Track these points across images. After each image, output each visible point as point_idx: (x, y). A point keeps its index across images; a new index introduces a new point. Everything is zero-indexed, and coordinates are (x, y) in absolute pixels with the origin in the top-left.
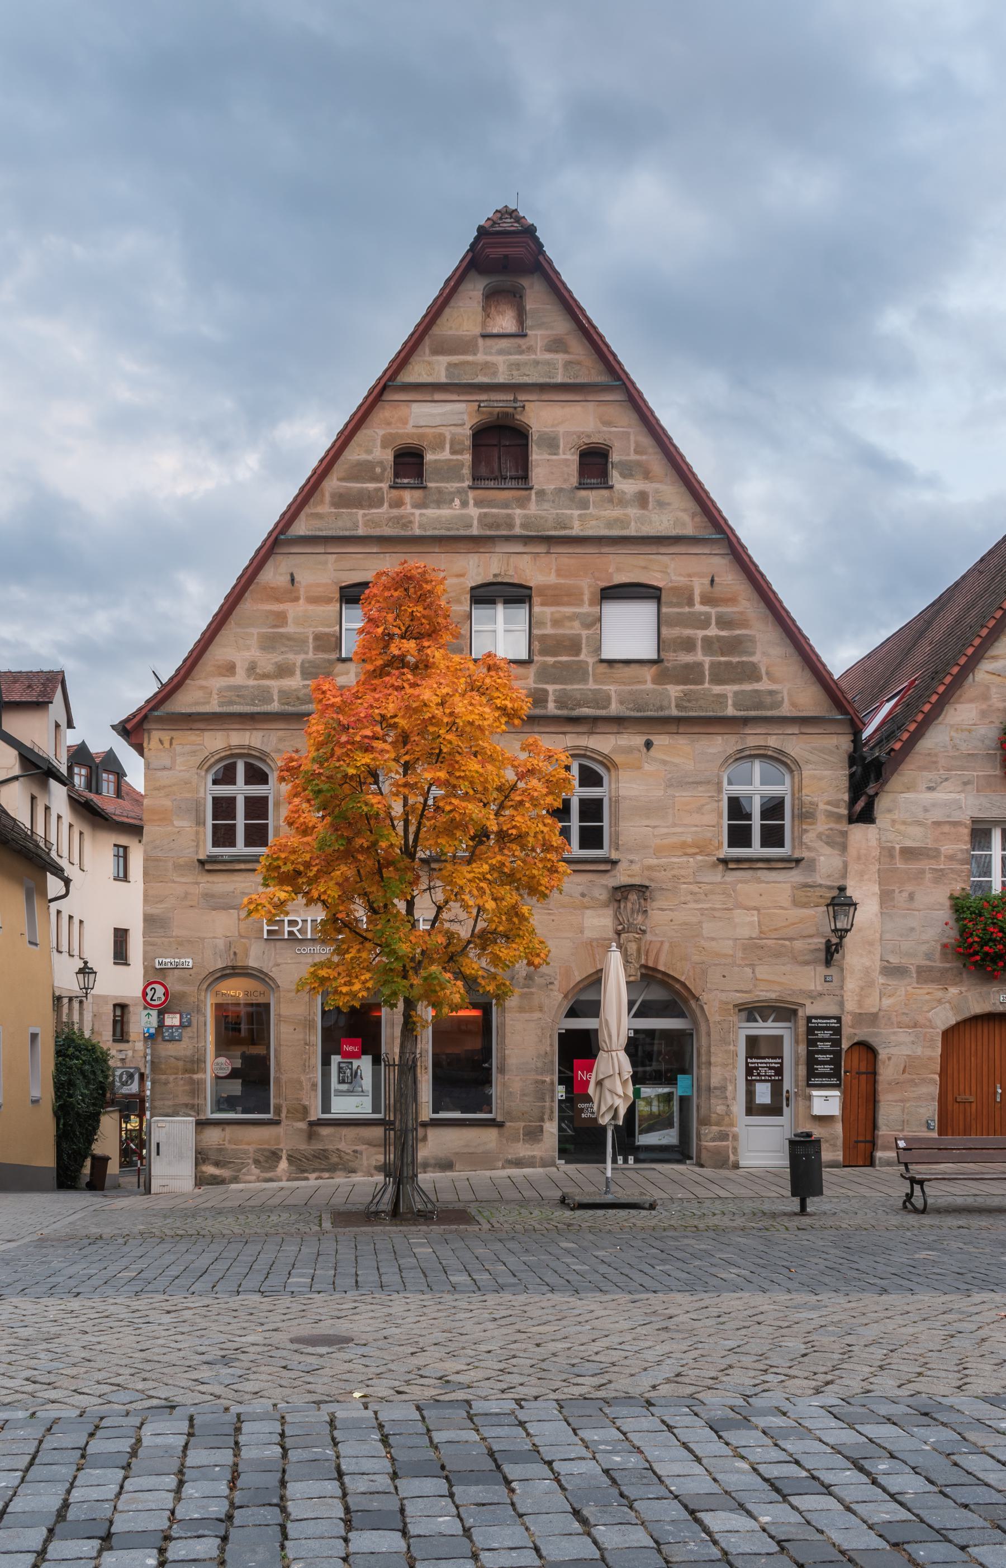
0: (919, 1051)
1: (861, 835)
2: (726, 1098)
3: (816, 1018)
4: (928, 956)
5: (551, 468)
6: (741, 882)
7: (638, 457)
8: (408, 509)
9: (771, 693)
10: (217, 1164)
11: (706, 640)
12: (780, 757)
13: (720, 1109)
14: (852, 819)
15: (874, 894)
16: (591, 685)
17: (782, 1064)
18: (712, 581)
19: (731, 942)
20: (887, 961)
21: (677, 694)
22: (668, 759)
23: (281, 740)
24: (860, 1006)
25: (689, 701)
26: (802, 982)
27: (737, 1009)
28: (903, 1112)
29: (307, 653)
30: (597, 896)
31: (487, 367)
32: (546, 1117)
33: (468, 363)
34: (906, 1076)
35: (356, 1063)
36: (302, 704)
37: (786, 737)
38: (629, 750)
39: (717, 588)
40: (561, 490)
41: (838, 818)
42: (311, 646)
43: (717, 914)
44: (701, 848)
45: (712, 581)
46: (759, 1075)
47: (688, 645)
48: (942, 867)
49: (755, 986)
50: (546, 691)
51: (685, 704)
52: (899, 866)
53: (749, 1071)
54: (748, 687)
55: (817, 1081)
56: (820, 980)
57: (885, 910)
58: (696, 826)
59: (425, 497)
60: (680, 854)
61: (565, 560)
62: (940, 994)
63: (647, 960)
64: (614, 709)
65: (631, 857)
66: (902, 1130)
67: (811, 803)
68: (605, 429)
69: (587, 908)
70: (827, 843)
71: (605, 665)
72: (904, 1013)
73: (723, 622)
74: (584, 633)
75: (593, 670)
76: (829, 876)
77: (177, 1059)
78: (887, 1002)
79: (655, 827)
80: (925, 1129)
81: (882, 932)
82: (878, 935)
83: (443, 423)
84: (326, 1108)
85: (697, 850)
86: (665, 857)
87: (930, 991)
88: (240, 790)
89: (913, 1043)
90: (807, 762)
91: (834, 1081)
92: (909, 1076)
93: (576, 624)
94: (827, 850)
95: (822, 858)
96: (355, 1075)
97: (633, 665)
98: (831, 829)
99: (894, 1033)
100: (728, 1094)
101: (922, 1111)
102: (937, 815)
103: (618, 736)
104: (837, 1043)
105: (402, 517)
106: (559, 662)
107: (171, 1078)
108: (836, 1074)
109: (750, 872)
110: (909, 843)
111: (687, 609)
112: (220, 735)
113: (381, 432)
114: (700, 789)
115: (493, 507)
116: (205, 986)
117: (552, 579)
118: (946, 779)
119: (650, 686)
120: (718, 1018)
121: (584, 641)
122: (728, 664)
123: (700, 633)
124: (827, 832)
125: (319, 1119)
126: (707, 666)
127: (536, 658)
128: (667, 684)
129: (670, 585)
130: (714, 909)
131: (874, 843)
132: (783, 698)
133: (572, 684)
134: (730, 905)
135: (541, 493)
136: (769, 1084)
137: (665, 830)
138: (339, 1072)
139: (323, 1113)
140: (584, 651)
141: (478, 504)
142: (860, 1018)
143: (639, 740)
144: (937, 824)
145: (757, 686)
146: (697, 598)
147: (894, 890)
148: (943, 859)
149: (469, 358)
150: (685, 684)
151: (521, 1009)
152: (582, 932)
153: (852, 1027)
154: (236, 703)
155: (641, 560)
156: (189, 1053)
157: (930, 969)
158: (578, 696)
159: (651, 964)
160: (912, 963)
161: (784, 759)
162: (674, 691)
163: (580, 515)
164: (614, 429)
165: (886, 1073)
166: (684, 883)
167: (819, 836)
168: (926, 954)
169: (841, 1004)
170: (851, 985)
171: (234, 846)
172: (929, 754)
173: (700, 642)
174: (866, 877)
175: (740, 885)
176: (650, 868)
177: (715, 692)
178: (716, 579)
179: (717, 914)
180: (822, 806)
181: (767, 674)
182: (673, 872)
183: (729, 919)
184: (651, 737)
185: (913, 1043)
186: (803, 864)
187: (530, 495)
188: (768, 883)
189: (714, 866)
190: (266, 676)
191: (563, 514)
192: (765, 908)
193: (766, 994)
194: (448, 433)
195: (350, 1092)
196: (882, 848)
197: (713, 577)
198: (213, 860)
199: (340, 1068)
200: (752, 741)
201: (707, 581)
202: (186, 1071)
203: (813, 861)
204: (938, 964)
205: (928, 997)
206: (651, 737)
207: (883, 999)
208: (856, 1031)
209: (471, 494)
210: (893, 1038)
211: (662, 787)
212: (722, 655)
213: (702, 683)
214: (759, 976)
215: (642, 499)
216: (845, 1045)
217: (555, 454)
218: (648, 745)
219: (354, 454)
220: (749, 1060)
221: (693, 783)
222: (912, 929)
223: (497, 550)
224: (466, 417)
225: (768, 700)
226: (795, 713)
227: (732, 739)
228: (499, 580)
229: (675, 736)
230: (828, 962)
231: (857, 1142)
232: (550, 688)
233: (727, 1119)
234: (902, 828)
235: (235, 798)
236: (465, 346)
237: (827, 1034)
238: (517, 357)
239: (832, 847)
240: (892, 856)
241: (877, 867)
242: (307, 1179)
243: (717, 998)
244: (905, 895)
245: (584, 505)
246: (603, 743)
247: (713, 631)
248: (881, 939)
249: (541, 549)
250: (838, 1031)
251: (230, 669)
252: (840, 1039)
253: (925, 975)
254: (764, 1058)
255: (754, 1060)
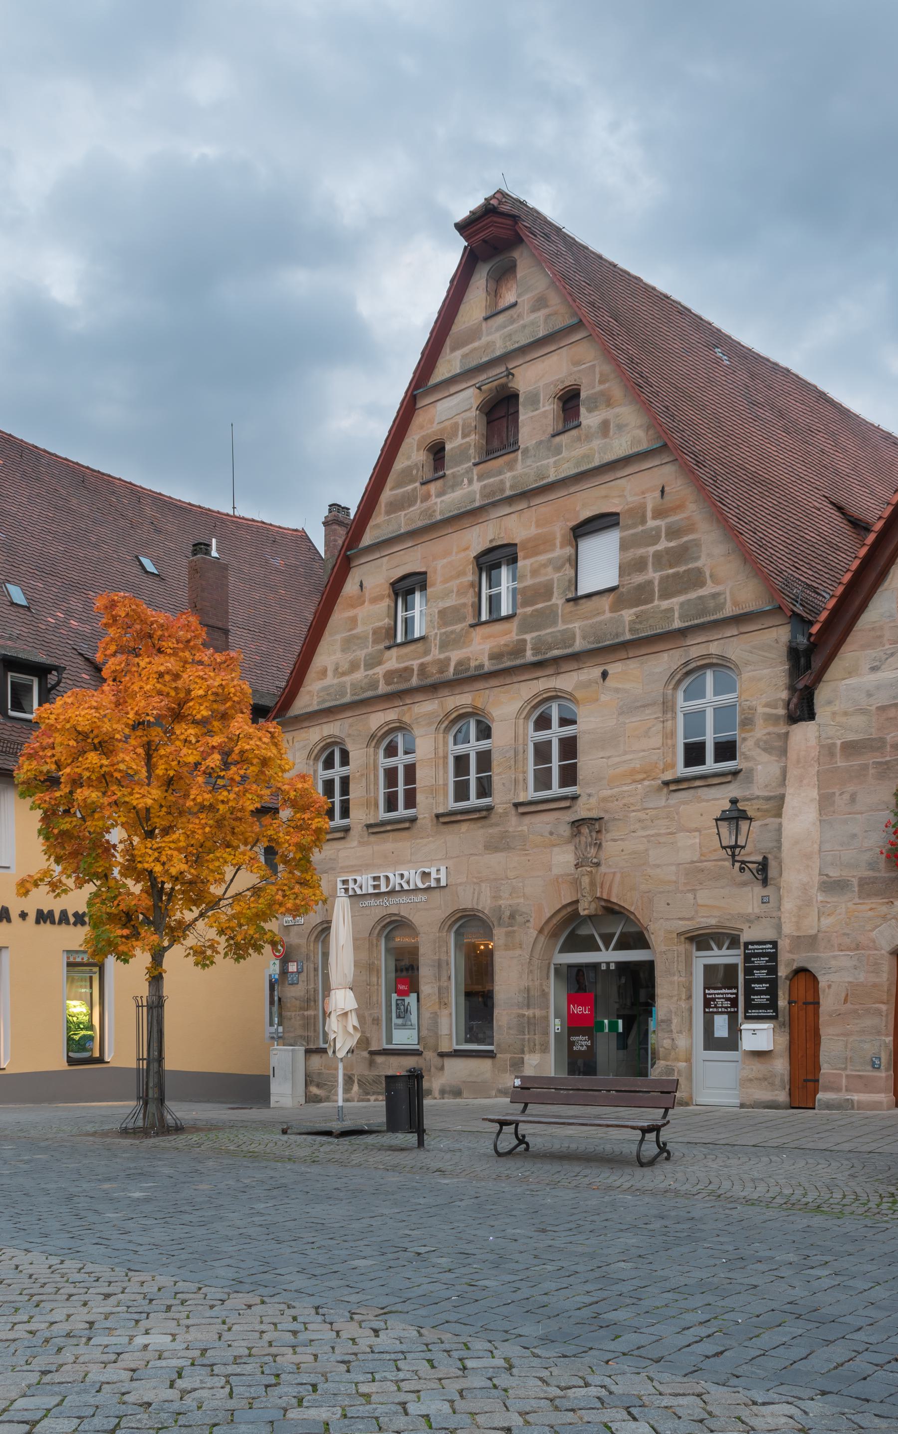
0: (862, 977)
1: (804, 735)
2: (671, 1031)
3: (753, 943)
4: (872, 866)
5: (535, 421)
6: (684, 803)
7: (602, 387)
8: (433, 500)
9: (715, 596)
10: (318, 1086)
11: (657, 556)
12: (724, 663)
13: (667, 1043)
14: (793, 719)
15: (812, 800)
16: (561, 627)
17: (737, 994)
18: (663, 491)
19: (674, 868)
20: (827, 875)
21: (630, 618)
22: (620, 686)
23: (351, 726)
24: (798, 928)
25: (640, 623)
26: (734, 904)
27: (682, 938)
28: (846, 1047)
29: (368, 648)
30: (562, 833)
31: (490, 345)
32: (526, 1049)
33: (475, 349)
34: (849, 1006)
35: (407, 1000)
36: (363, 692)
37: (727, 640)
38: (587, 685)
39: (667, 497)
40: (541, 442)
41: (775, 719)
42: (371, 640)
43: (662, 840)
44: (648, 773)
45: (663, 491)
46: (716, 1007)
47: (494, 601)
48: (888, 758)
49: (696, 912)
50: (525, 641)
51: (637, 626)
52: (839, 764)
53: (707, 1003)
54: (693, 595)
55: (754, 1013)
56: (757, 902)
57: (824, 817)
58: (644, 751)
59: (444, 486)
60: (629, 781)
61: (543, 509)
62: (884, 909)
63: (602, 892)
64: (579, 645)
65: (589, 791)
66: (845, 1069)
67: (750, 708)
68: (576, 369)
69: (554, 846)
70: (765, 750)
71: (571, 603)
72: (844, 934)
73: (673, 533)
74: (556, 576)
75: (562, 611)
76: (766, 786)
77: (296, 999)
78: (826, 922)
79: (609, 757)
80: (870, 1068)
81: (821, 842)
82: (816, 847)
83: (455, 412)
84: (389, 1040)
85: (645, 776)
86: (617, 786)
87: (873, 906)
88: (555, 733)
89: (855, 968)
90: (747, 663)
91: (770, 1013)
92: (852, 1006)
93: (550, 569)
94: (765, 757)
95: (759, 767)
96: (406, 1011)
97: (594, 598)
98: (769, 734)
99: (835, 957)
100: (673, 1027)
101: (867, 1046)
102: (883, 699)
103: (580, 671)
104: (773, 970)
105: (429, 508)
106: (536, 610)
107: (293, 1014)
108: (773, 1004)
109: (692, 791)
110: (852, 737)
111: (640, 528)
112: (317, 728)
113: (417, 437)
114: (647, 712)
115: (490, 477)
116: (313, 939)
117: (533, 531)
118: (892, 654)
119: (608, 615)
120: (664, 948)
121: (555, 585)
122: (676, 574)
123: (651, 550)
124: (764, 738)
125: (384, 1050)
126: (656, 583)
127: (518, 611)
128: (622, 609)
129: (626, 507)
130: (659, 835)
131: (813, 742)
132: (725, 598)
133: (545, 629)
134: (673, 830)
135: (526, 451)
136: (726, 1017)
137: (617, 759)
138: (397, 1008)
139: (457, 1044)
140: (555, 594)
141: (481, 478)
142: (799, 942)
143: (597, 672)
144: (882, 709)
145: (702, 592)
146: (649, 514)
147: (834, 793)
148: (888, 748)
149: (476, 344)
150: (637, 606)
151: (507, 947)
152: (550, 870)
153: (790, 952)
154: (327, 701)
155: (602, 491)
156: (302, 994)
157: (874, 881)
158: (550, 640)
159: (605, 897)
160: (853, 876)
161: (728, 664)
162: (628, 614)
163: (555, 462)
164: (583, 366)
165: (828, 1003)
166: (634, 811)
167: (757, 744)
168: (870, 864)
169: (779, 927)
170: (789, 905)
171: (469, 799)
172: (873, 629)
173: (651, 559)
174: (805, 782)
175: (682, 807)
176: (605, 800)
177: (663, 608)
178: (666, 489)
179: (662, 840)
180: (761, 710)
181: (711, 576)
182: (624, 801)
183: (672, 843)
184: (607, 667)
185: (855, 968)
186: (741, 775)
187: (517, 456)
188: (708, 801)
189: (659, 789)
190: (343, 674)
191: (541, 465)
192: (706, 829)
193: (707, 920)
194: (459, 420)
195: (404, 1025)
196: (822, 746)
197: (663, 487)
198: (383, 823)
199: (397, 1005)
200: (695, 652)
201: (658, 494)
202: (301, 1009)
203: (751, 771)
204: (884, 874)
205: (870, 913)
206: (607, 667)
207: (822, 919)
208: (795, 957)
209: (475, 471)
210: (833, 963)
211: (615, 716)
212: (671, 567)
213: (652, 601)
214: (700, 901)
215: (605, 426)
216: (783, 972)
217: (537, 410)
218: (605, 675)
219: (400, 464)
220: (707, 991)
221: (641, 706)
222: (854, 836)
223: (492, 516)
224: (473, 400)
225: (711, 604)
226: (738, 611)
227: (676, 653)
228: (494, 544)
229: (628, 662)
230: (765, 882)
231: (806, 1081)
232: (528, 637)
233: (673, 1053)
234: (843, 720)
235: (469, 754)
236: (474, 334)
237: (763, 961)
238: (511, 327)
239: (770, 753)
240: (832, 754)
241: (816, 769)
242: (369, 1100)
243: (663, 929)
244: (846, 797)
245: (558, 450)
246: (566, 682)
247: (663, 545)
248: (820, 850)
249: (523, 505)
250: (773, 957)
251: (324, 673)
252: (776, 966)
253: (868, 888)
254: (720, 989)
255: (712, 991)
